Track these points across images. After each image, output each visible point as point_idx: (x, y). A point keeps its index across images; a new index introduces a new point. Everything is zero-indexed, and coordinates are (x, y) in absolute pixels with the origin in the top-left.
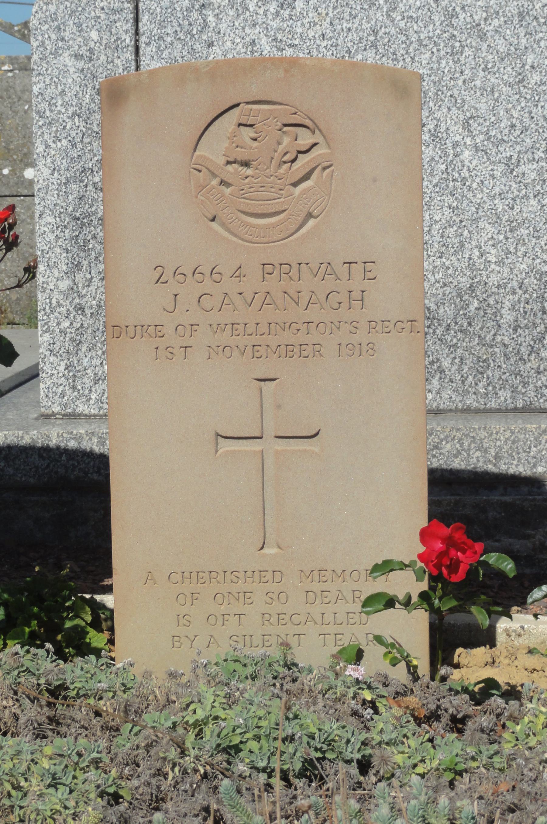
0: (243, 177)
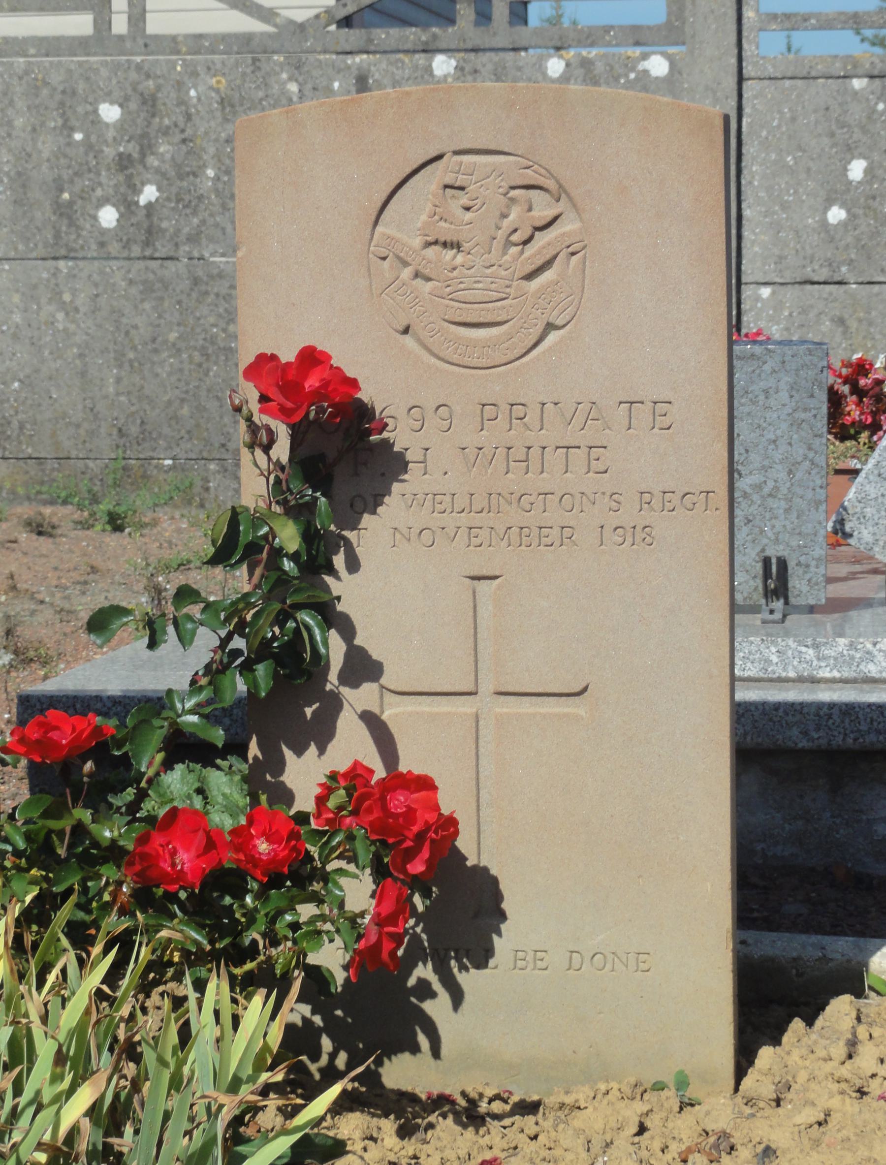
0: (449, 267)
